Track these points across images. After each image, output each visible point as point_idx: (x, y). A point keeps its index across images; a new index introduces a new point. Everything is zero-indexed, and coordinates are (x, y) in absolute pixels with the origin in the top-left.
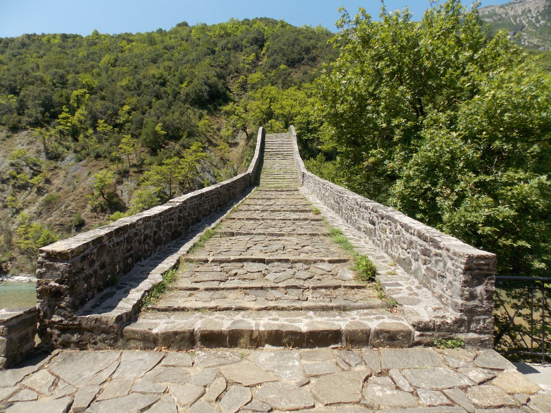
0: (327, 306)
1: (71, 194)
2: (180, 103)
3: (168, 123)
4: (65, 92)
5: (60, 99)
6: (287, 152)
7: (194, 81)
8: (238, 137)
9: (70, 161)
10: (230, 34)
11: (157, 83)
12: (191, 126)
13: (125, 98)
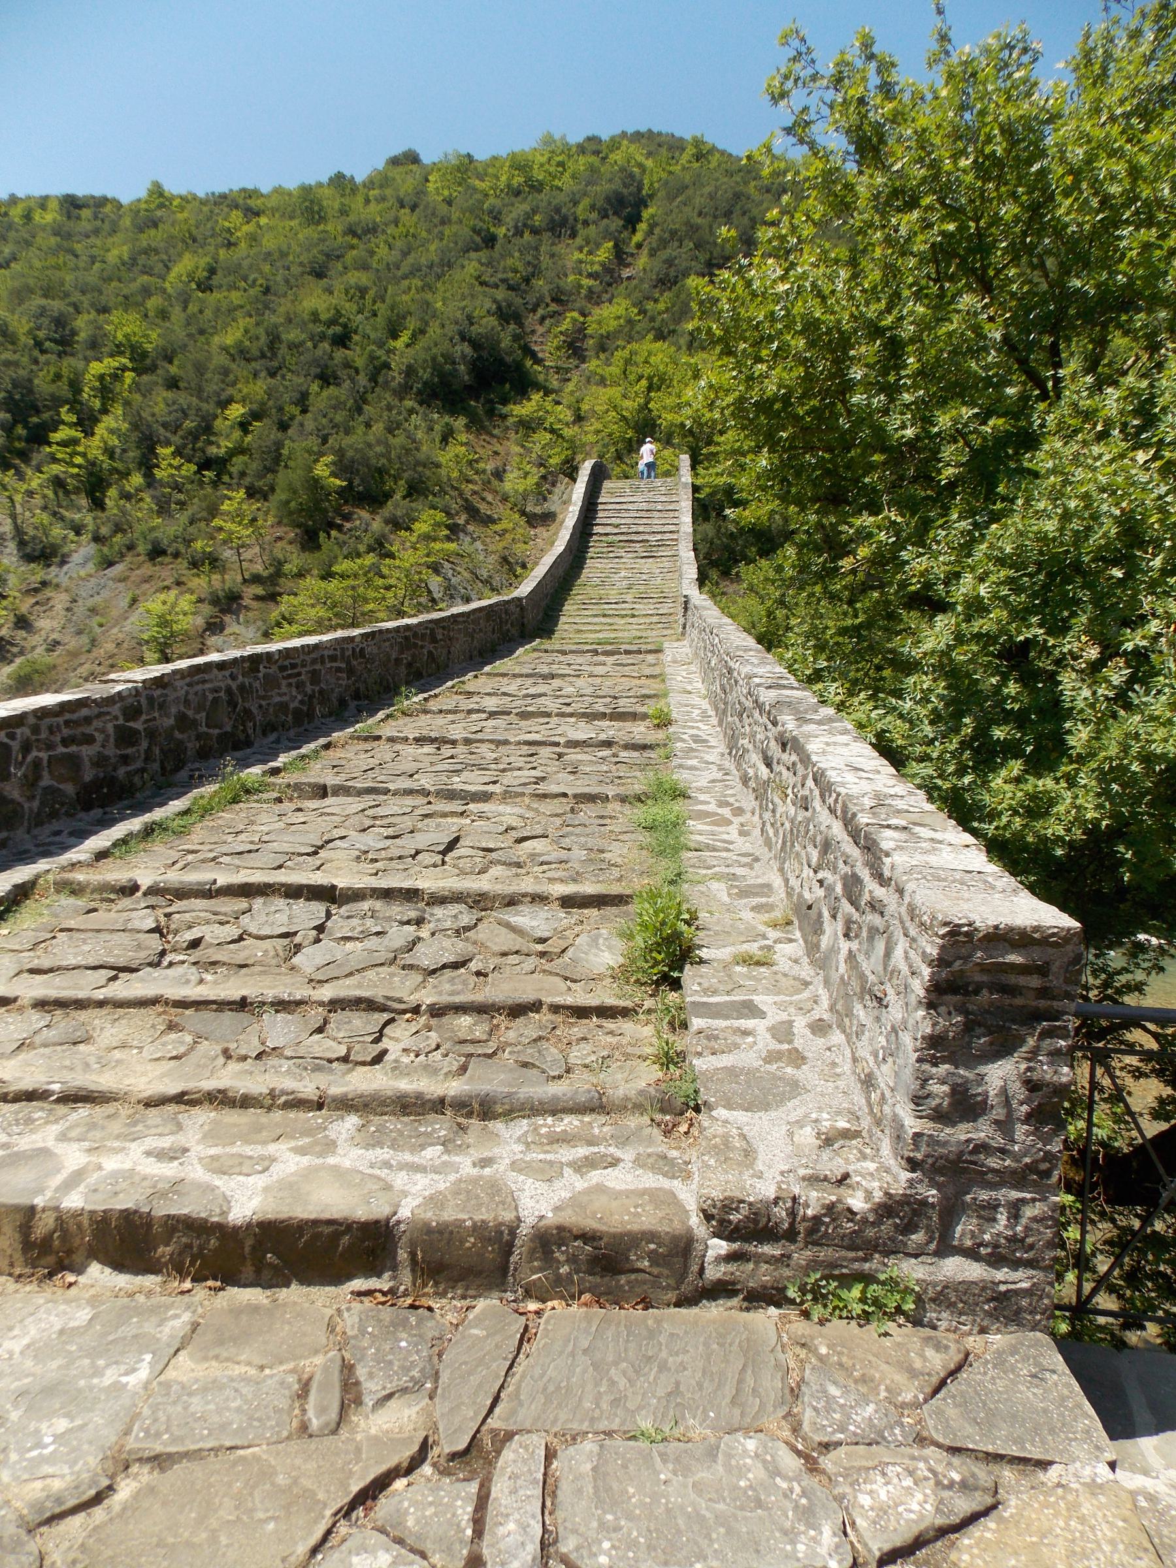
0: (419, 1096)
1: (82, 659)
2: (387, 395)
3: (350, 453)
4: (68, 364)
5: (52, 388)
6: (659, 537)
7: (430, 330)
8: (556, 498)
9: (84, 564)
10: (541, 184)
11: (323, 337)
12: (418, 463)
13: (234, 384)
